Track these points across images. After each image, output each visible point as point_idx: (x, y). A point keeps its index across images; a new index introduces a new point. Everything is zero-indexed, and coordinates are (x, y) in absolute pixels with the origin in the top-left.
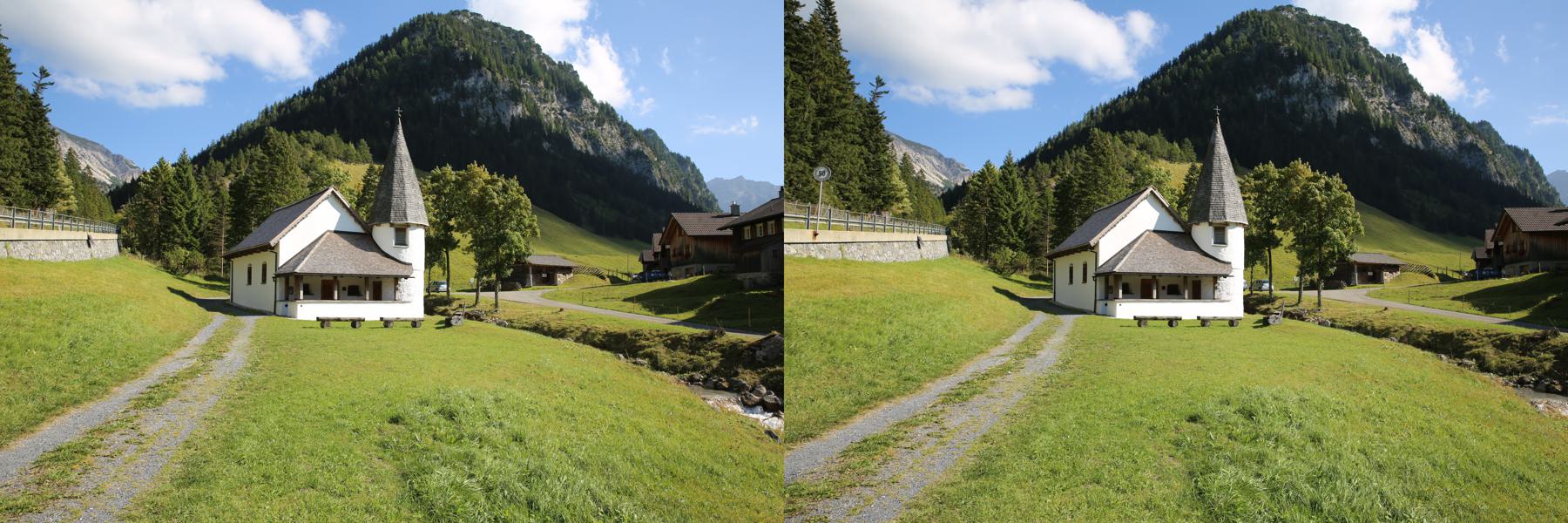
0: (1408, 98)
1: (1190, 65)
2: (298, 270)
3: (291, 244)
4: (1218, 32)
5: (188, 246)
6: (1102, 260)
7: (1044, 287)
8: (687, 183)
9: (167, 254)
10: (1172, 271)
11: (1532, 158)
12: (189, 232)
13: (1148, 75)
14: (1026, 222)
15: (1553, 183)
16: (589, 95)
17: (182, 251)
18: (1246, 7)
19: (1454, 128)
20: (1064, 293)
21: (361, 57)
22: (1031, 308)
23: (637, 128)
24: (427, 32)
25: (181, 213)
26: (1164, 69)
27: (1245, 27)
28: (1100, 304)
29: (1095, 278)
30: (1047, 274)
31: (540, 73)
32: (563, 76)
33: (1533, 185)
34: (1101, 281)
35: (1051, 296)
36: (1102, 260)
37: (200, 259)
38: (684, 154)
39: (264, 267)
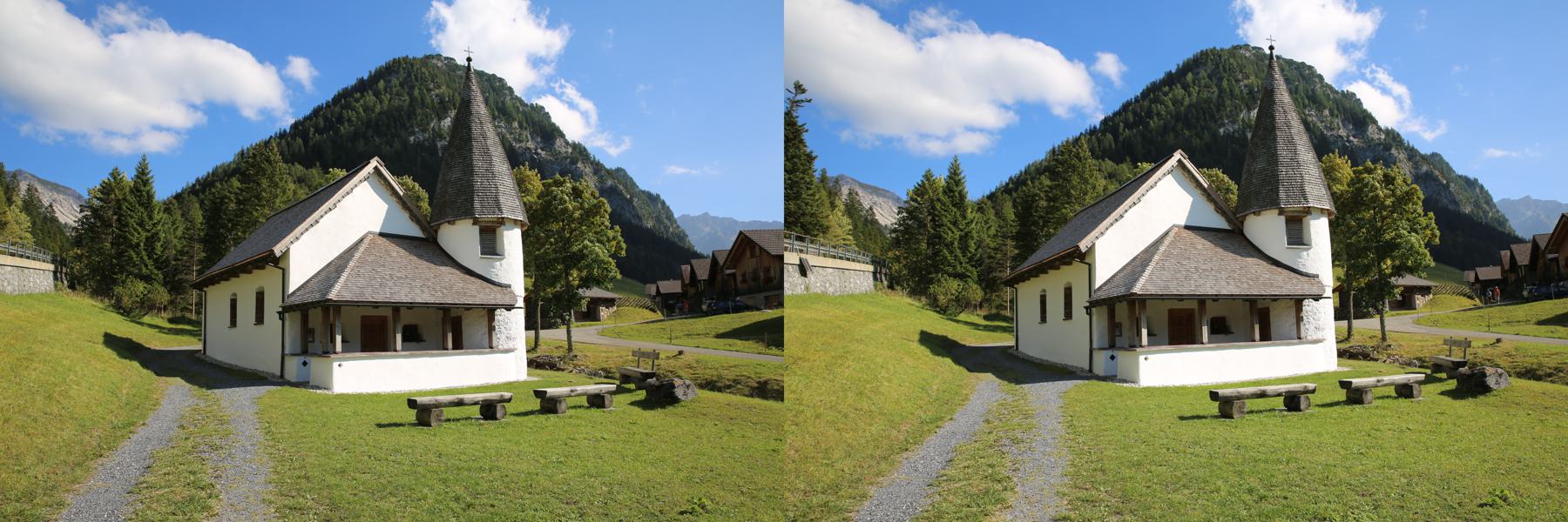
0: (1365, 131)
1: (343, 108)
2: (333, 295)
3: (309, 252)
4: (1178, 70)
5: (147, 279)
6: (1102, 275)
7: (1004, 329)
8: (1477, 205)
9: (118, 290)
10: (431, 300)
11: (1482, 187)
12: (150, 263)
13: (300, 118)
14: (165, 247)
15: (683, 226)
16: (1375, 122)
17: (141, 287)
18: (1206, 46)
19: (1410, 159)
20: (225, 341)
21: (337, 99)
22: (936, 352)
23: (1422, 152)
24: (403, 75)
25: (953, 235)
26: (1125, 107)
27: (1205, 64)
28: (1101, 358)
29: (1088, 310)
30: (1008, 313)
31: (1325, 102)
32: (1347, 104)
33: (667, 228)
34: (1100, 317)
35: (199, 346)
36: (1102, 275)
37: (163, 295)
38: (1471, 176)
39: (260, 297)
